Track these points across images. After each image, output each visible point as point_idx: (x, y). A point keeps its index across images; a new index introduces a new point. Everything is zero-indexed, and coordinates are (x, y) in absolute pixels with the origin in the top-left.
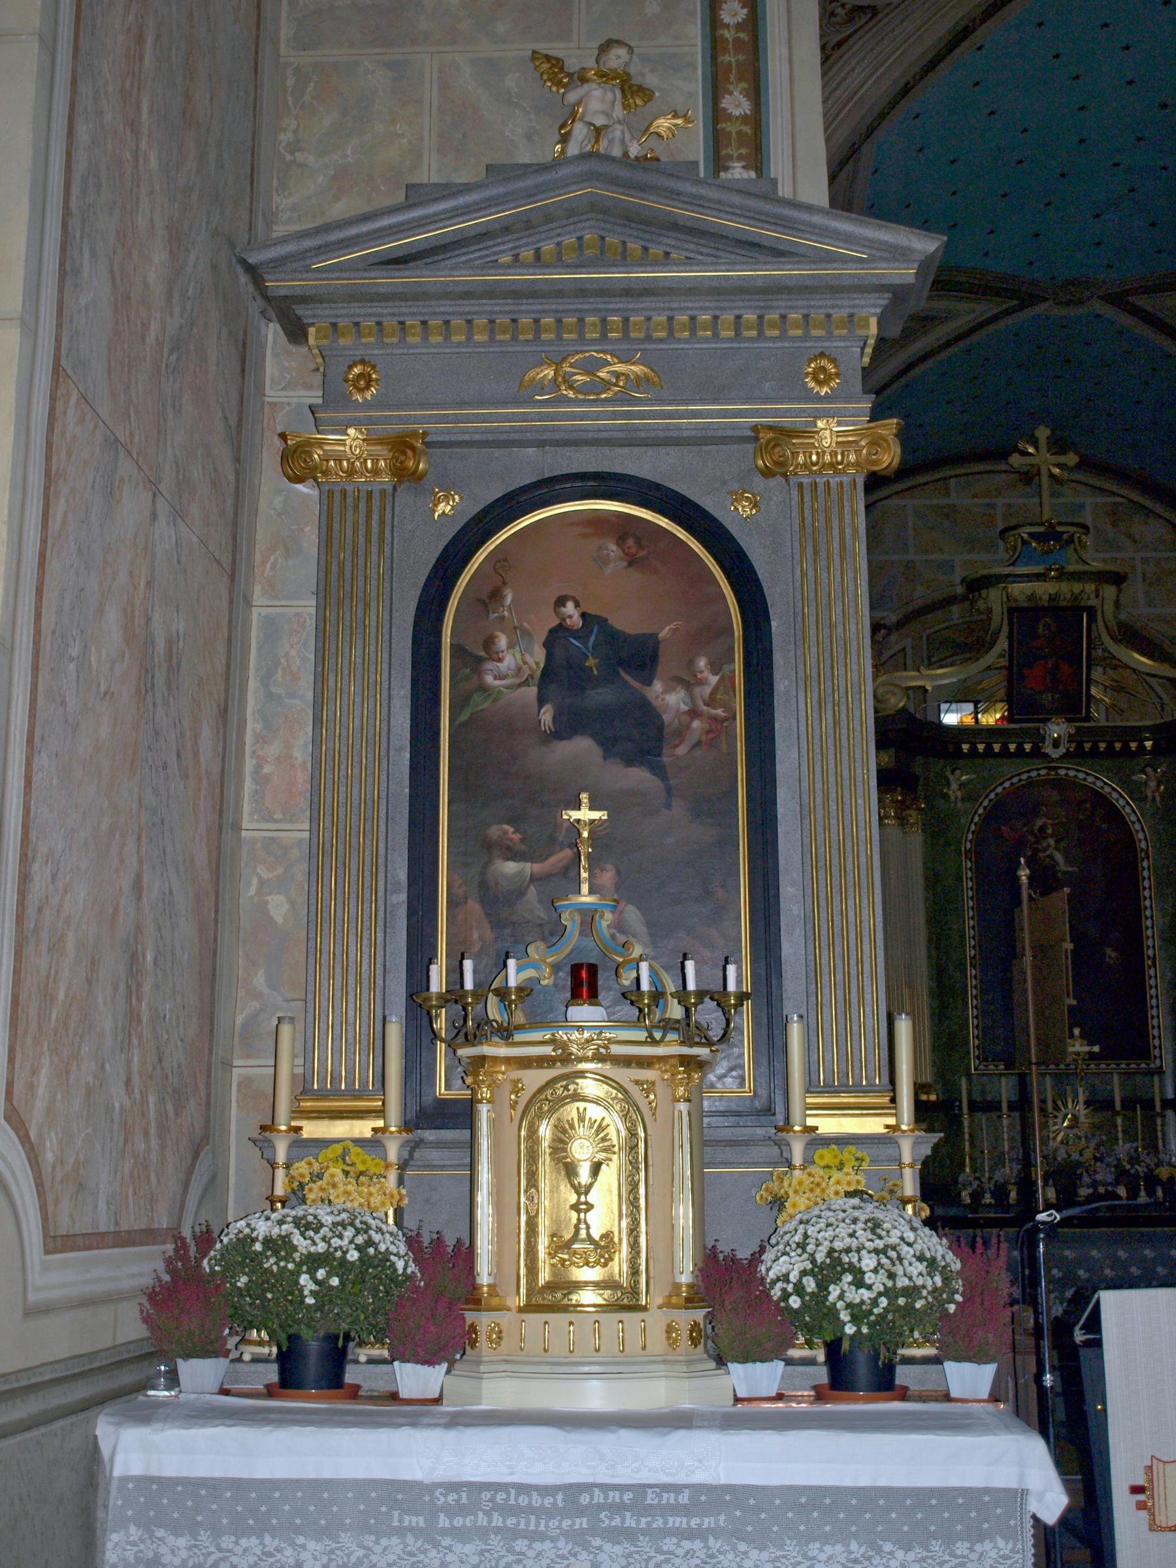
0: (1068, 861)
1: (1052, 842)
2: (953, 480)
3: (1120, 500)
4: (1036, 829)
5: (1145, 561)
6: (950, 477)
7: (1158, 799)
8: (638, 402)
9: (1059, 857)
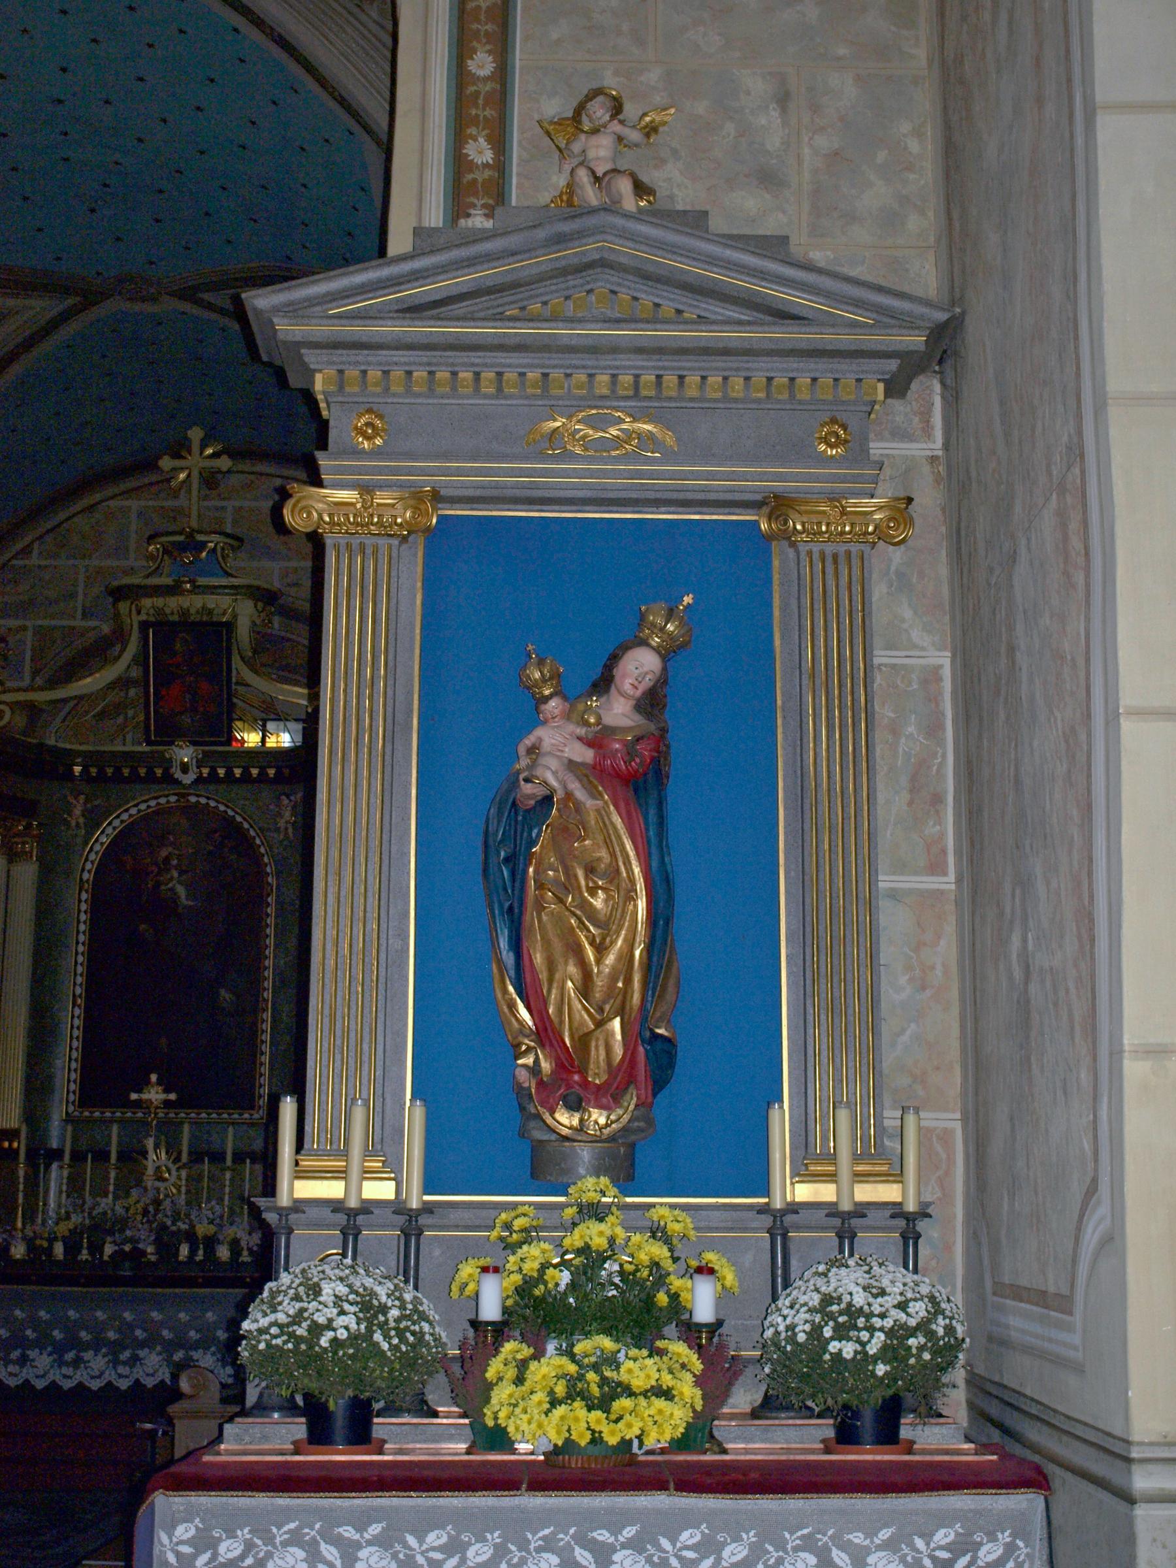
1: (175, 874)
4: (160, 859)
7: (290, 831)
8: (653, 461)
9: (181, 891)
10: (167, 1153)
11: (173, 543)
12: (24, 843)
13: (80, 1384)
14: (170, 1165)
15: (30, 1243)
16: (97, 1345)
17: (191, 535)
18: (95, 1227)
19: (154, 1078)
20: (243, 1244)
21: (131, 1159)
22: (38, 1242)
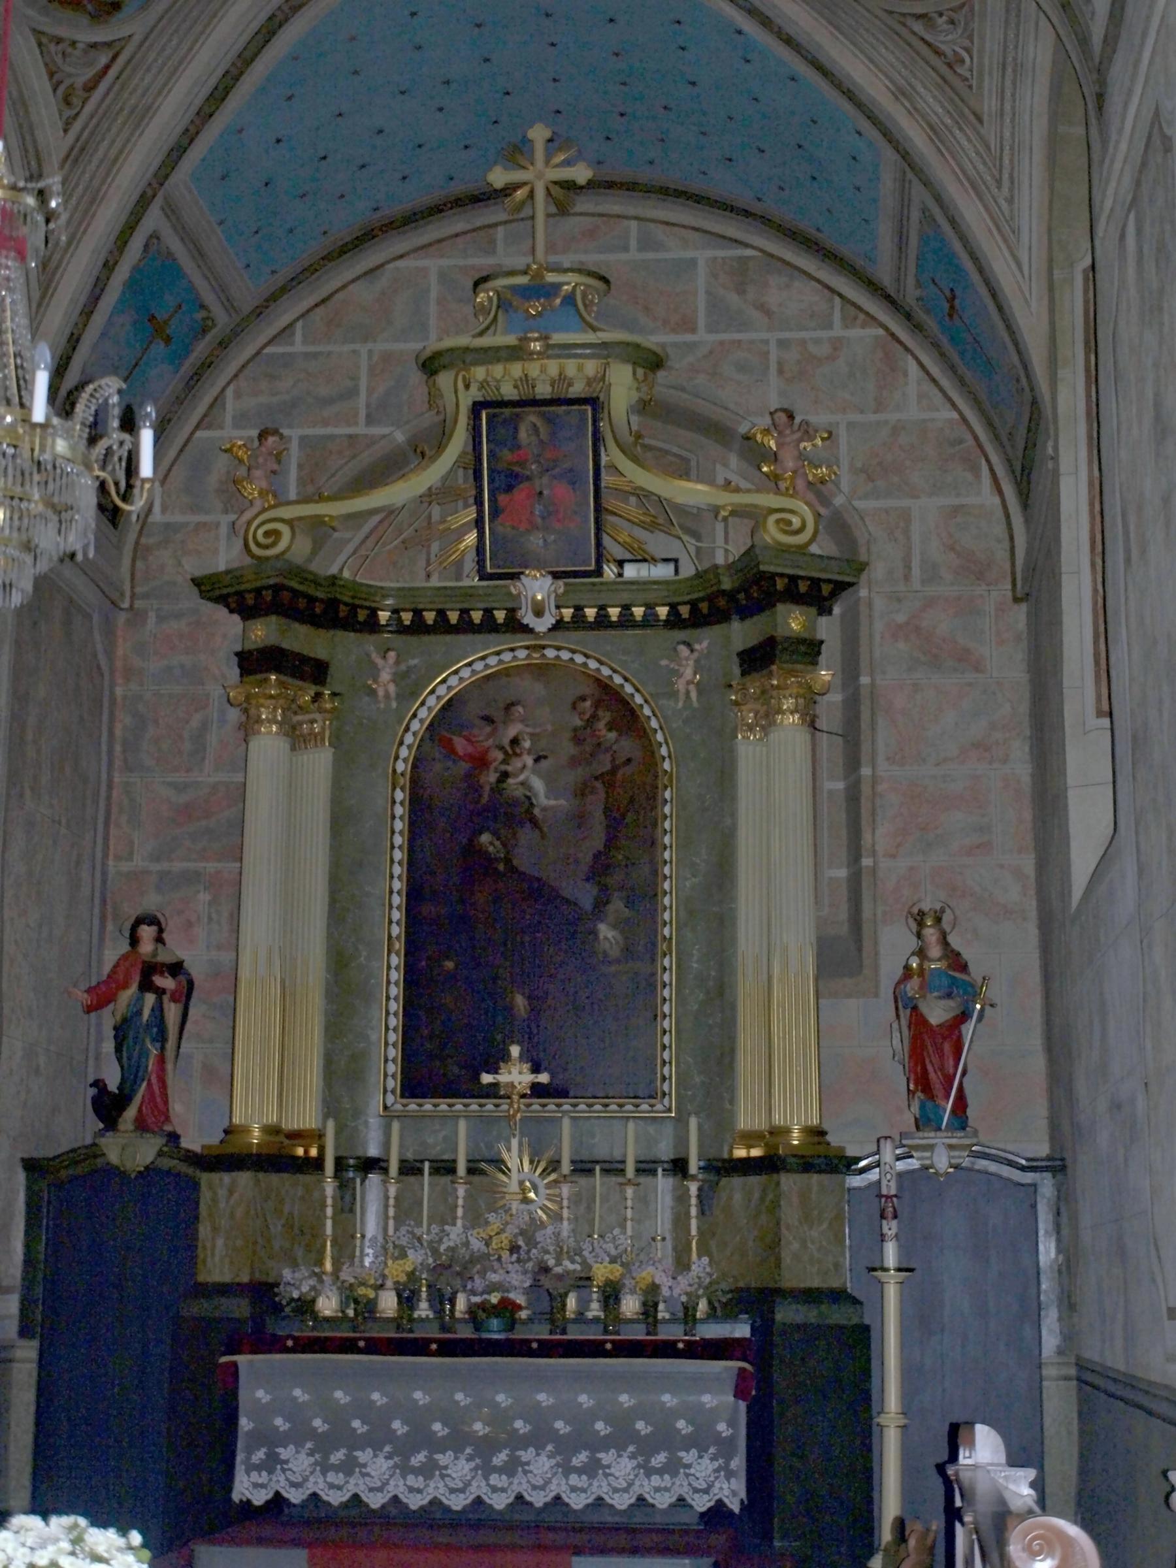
0: (551, 792)
1: (529, 761)
2: (500, 229)
3: (749, 252)
4: (506, 742)
5: (783, 344)
6: (496, 225)
7: (694, 695)
9: (538, 785)
10: (531, 1162)
11: (514, 289)
12: (312, 722)
13: (435, 1502)
14: (538, 1181)
15: (349, 1295)
16: (457, 1441)
17: (538, 275)
18: (440, 1269)
19: (515, 1050)
20: (665, 1292)
21: (482, 1172)
22: (362, 1291)
